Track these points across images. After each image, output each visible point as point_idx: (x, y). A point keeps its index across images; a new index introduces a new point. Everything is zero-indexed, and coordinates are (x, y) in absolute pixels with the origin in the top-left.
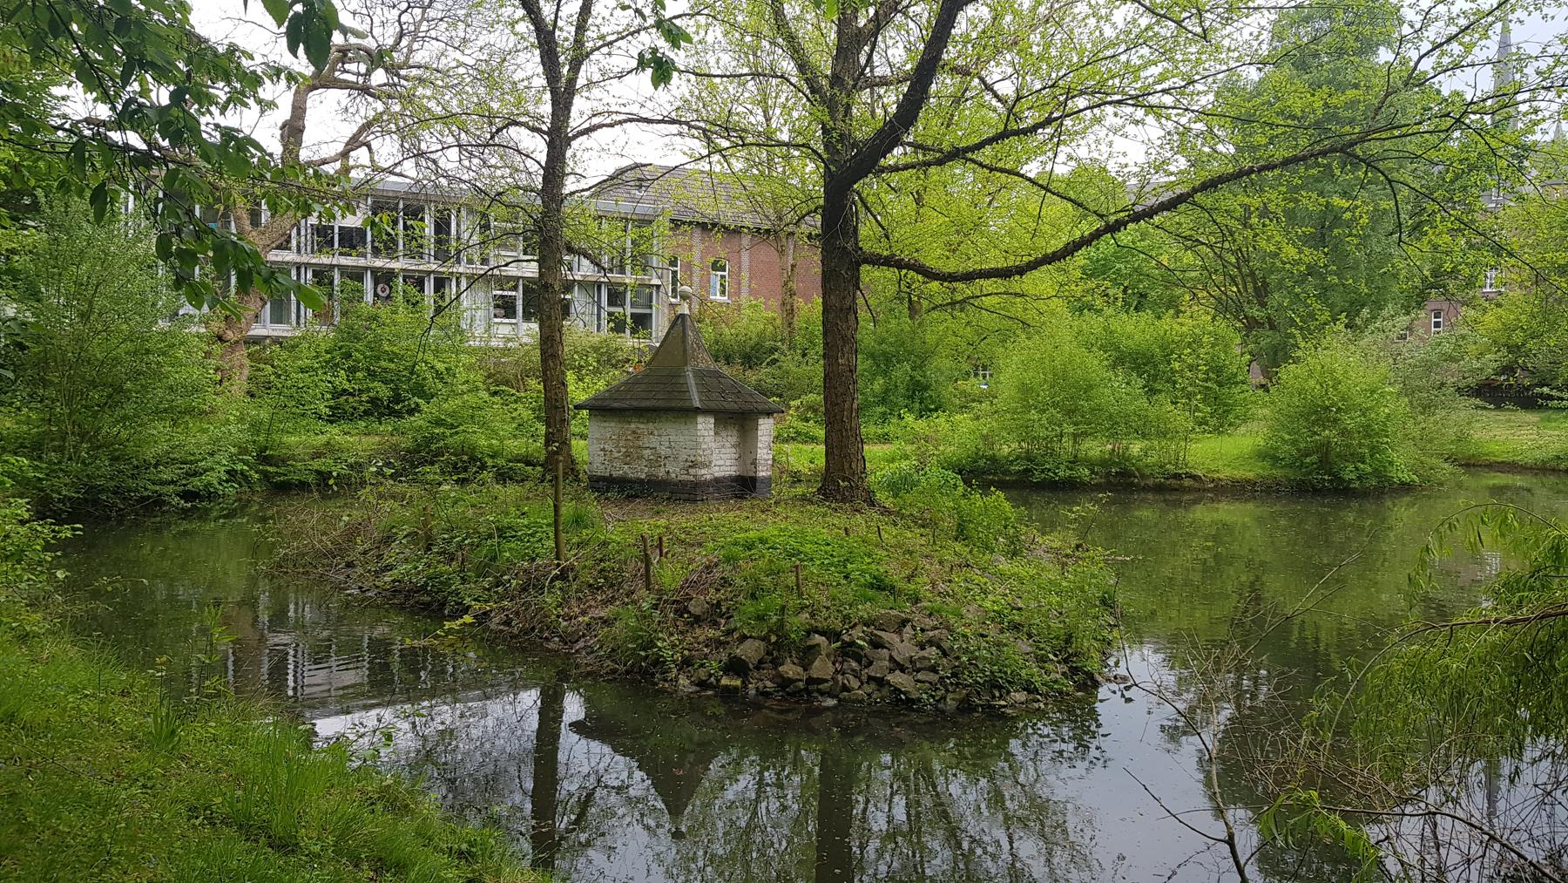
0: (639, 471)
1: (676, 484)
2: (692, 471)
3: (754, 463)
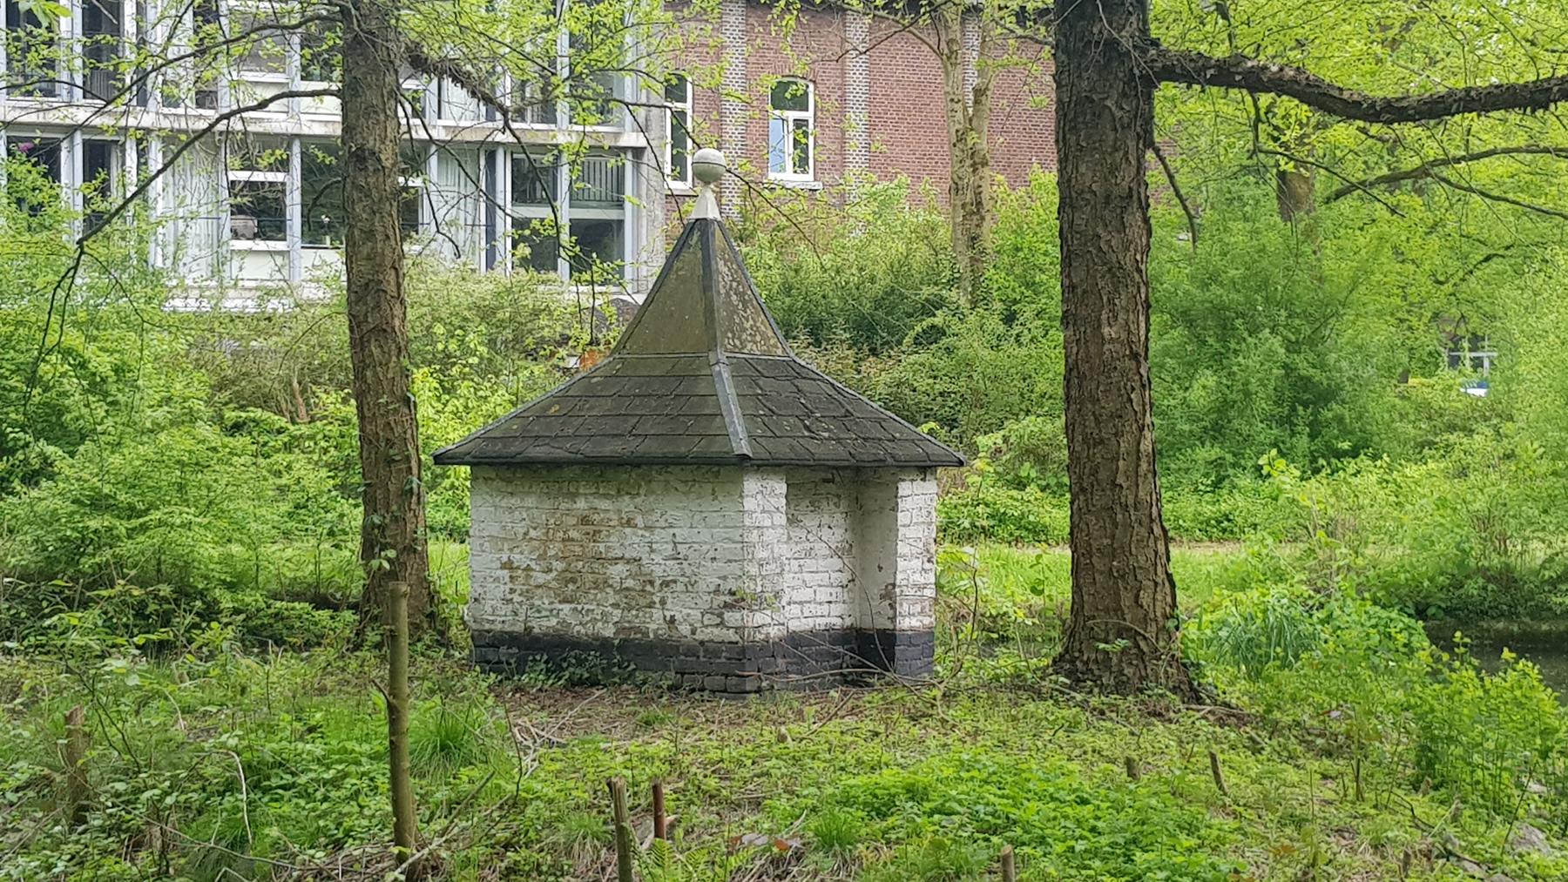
0: (598, 618)
3: (889, 594)
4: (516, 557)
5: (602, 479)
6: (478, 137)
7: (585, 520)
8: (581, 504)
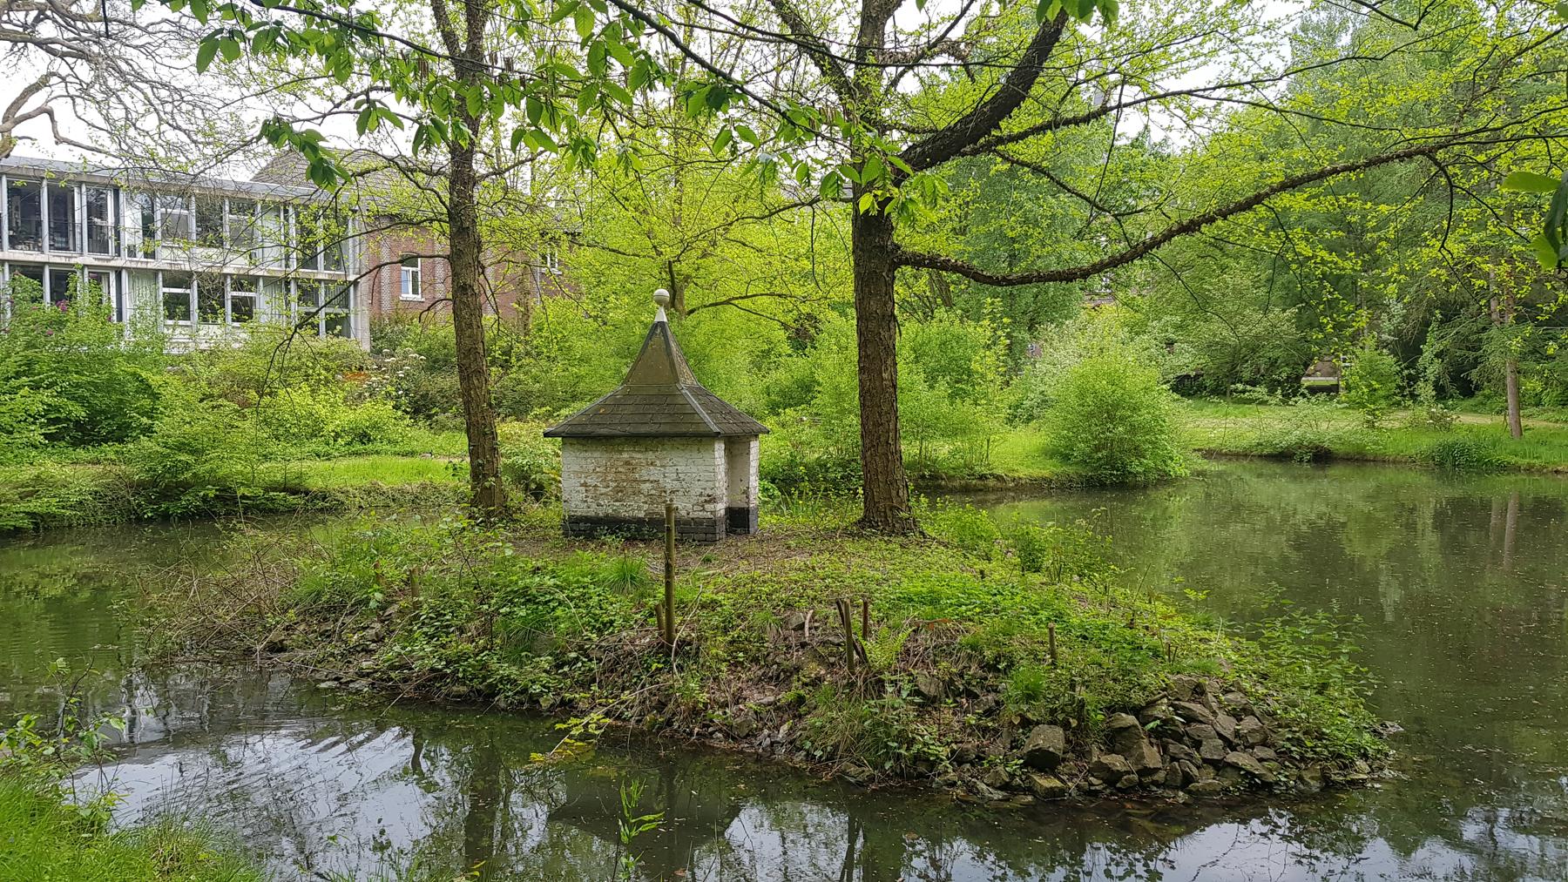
0: (637, 508)
1: (687, 523)
2: (707, 506)
3: (746, 492)
4: (589, 481)
5: (636, 443)
6: (281, 275)
7: (627, 463)
8: (625, 455)
